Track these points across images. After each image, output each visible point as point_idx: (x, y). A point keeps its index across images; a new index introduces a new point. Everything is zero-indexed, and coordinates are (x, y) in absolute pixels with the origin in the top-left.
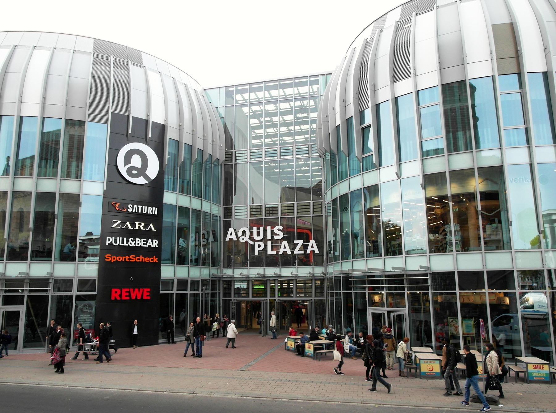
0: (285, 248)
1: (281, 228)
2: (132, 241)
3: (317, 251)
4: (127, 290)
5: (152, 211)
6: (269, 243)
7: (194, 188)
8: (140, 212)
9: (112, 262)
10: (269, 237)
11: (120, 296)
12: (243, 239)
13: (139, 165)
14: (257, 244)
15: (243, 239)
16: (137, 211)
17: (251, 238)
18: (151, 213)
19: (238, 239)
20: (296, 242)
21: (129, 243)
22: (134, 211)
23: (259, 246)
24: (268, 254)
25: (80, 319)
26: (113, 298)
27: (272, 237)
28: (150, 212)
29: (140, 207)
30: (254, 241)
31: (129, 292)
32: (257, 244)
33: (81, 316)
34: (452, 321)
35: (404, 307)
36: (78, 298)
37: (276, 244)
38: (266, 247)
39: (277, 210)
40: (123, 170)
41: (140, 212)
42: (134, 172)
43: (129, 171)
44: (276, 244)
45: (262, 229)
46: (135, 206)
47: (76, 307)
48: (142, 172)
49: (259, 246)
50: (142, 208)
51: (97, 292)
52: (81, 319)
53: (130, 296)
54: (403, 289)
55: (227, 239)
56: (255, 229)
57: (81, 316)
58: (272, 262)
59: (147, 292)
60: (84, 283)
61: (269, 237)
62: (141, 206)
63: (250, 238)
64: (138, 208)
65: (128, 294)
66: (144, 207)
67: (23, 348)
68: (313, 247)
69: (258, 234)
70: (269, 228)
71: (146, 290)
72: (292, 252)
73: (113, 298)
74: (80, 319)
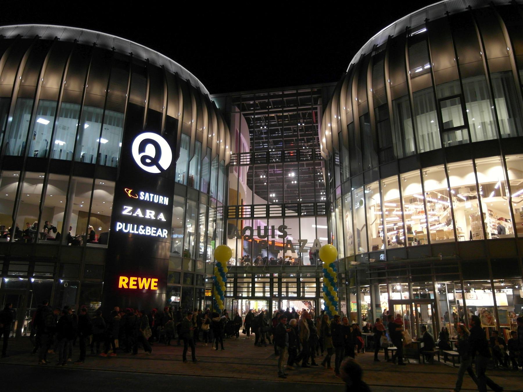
4: (136, 279)
5: (163, 201)
11: (128, 284)
28: (161, 201)
31: (137, 281)
42: (148, 161)
43: (143, 159)
50: (153, 197)
53: (137, 285)
59: (155, 282)
62: (153, 195)
64: (150, 196)
65: (135, 283)
66: (155, 195)
71: (154, 280)
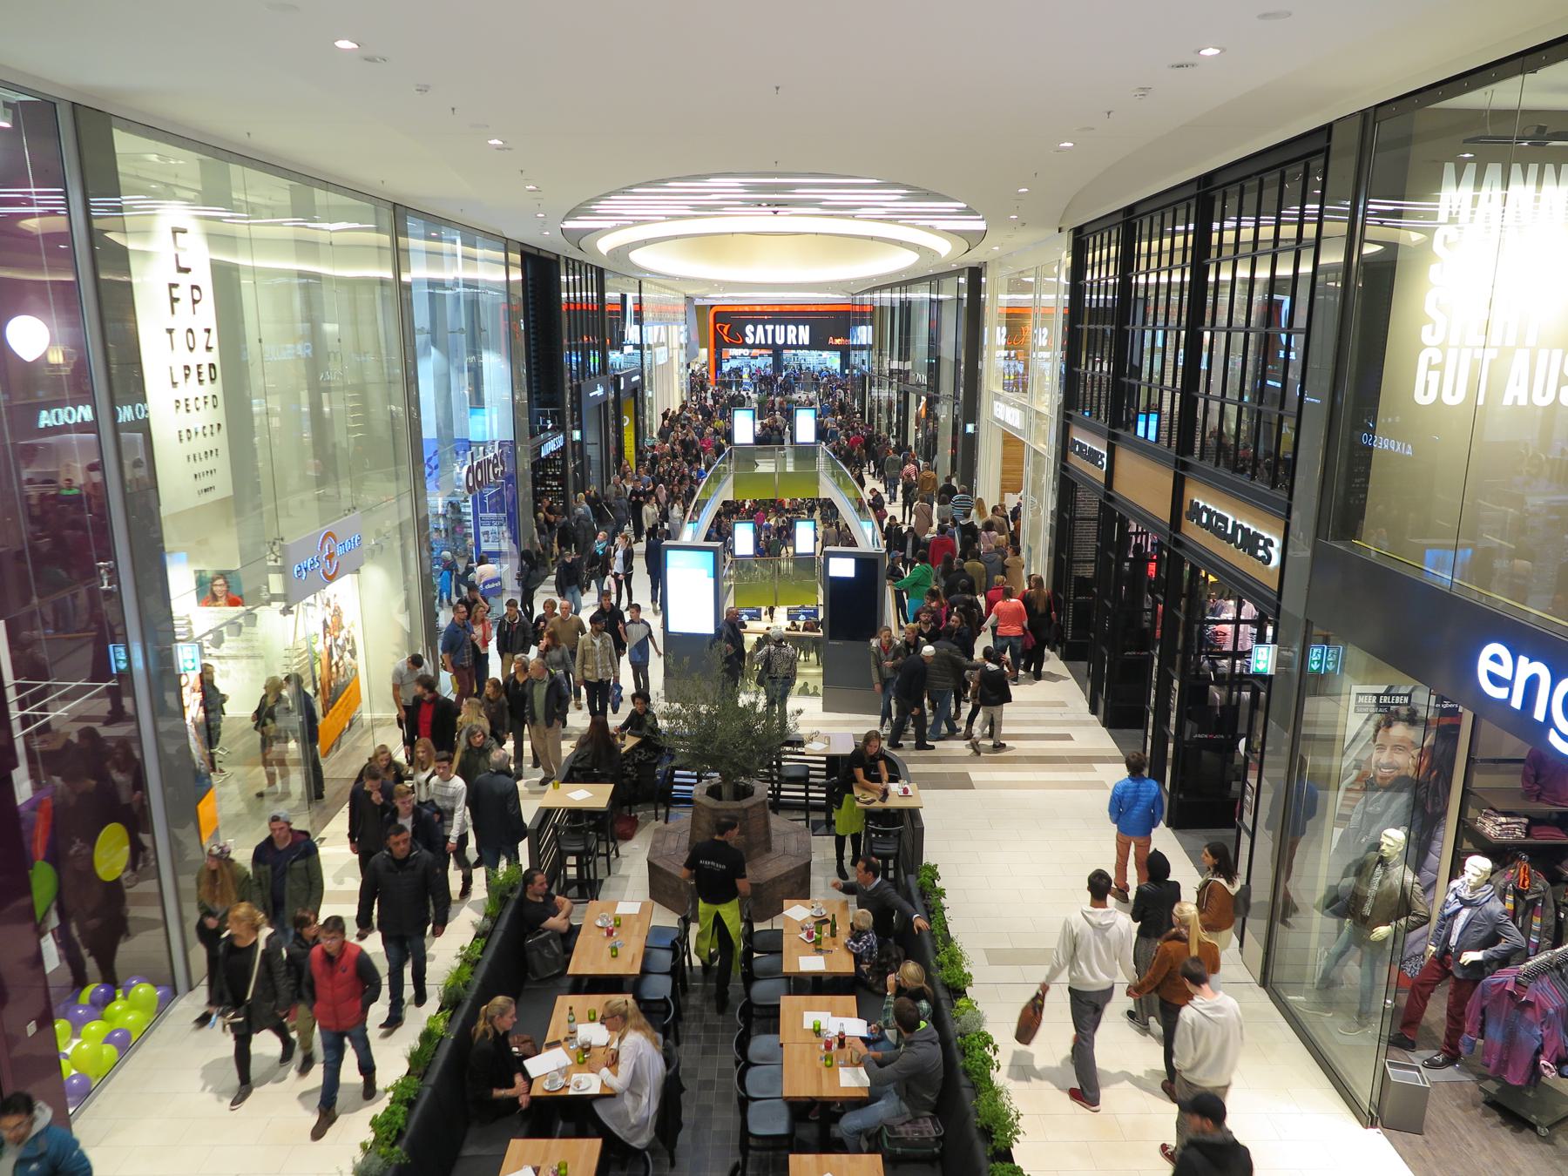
18: (795, 343)
29: (770, 328)
41: (770, 342)
46: (760, 328)
50: (774, 331)
66: (777, 327)
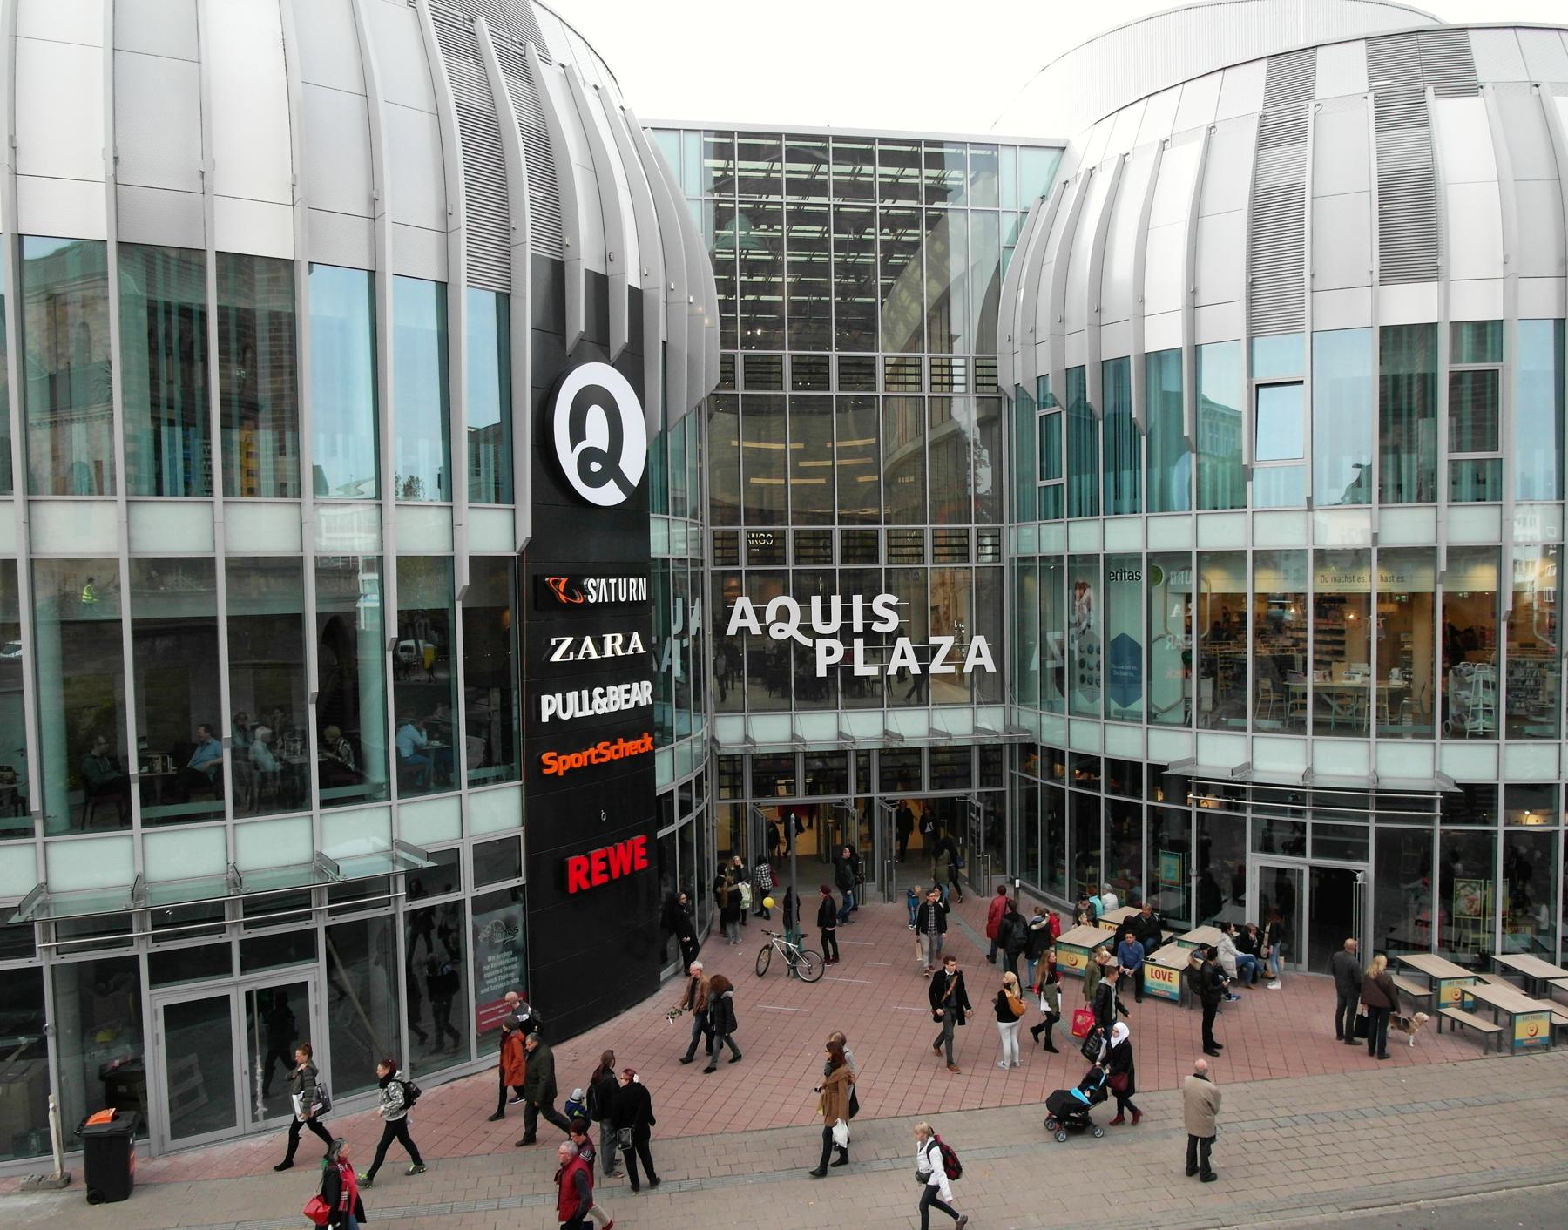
0: (903, 657)
1: (893, 600)
2: (603, 695)
3: (991, 667)
6: (859, 644)
7: (198, 366)
8: (613, 600)
9: (561, 774)
10: (858, 627)
12: (781, 631)
13: (603, 444)
14: (822, 645)
15: (781, 631)
16: (606, 600)
17: (806, 629)
19: (766, 629)
20: (933, 640)
21: (595, 704)
22: (600, 600)
23: (830, 652)
24: (857, 673)
25: (487, 971)
26: (573, 889)
27: (867, 627)
30: (817, 636)
32: (822, 645)
33: (490, 959)
34: (1463, 887)
35: (1365, 858)
36: (481, 905)
37: (878, 645)
38: (849, 656)
39: (889, 546)
40: (568, 459)
41: (613, 600)
44: (878, 645)
45: (836, 602)
47: (476, 932)
48: (607, 464)
49: (830, 652)
51: (529, 878)
52: (491, 970)
53: (608, 871)
54: (1365, 818)
55: (732, 630)
56: (816, 601)
57: (490, 959)
58: (858, 692)
60: (493, 857)
61: (858, 627)
63: (800, 628)
65: (603, 866)
67: (228, 996)
68: (980, 657)
69: (826, 616)
70: (858, 601)
72: (924, 669)
73: (573, 889)
74: (487, 971)
